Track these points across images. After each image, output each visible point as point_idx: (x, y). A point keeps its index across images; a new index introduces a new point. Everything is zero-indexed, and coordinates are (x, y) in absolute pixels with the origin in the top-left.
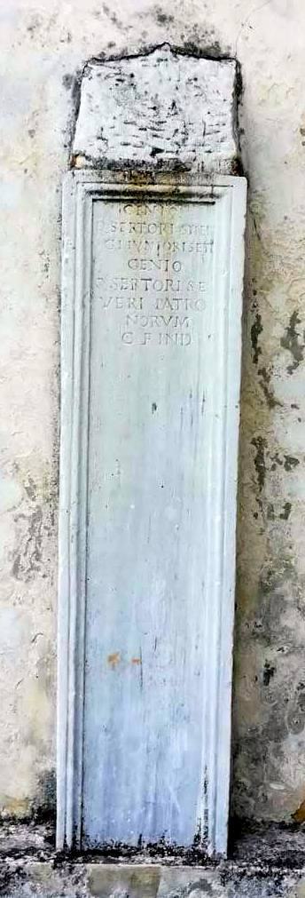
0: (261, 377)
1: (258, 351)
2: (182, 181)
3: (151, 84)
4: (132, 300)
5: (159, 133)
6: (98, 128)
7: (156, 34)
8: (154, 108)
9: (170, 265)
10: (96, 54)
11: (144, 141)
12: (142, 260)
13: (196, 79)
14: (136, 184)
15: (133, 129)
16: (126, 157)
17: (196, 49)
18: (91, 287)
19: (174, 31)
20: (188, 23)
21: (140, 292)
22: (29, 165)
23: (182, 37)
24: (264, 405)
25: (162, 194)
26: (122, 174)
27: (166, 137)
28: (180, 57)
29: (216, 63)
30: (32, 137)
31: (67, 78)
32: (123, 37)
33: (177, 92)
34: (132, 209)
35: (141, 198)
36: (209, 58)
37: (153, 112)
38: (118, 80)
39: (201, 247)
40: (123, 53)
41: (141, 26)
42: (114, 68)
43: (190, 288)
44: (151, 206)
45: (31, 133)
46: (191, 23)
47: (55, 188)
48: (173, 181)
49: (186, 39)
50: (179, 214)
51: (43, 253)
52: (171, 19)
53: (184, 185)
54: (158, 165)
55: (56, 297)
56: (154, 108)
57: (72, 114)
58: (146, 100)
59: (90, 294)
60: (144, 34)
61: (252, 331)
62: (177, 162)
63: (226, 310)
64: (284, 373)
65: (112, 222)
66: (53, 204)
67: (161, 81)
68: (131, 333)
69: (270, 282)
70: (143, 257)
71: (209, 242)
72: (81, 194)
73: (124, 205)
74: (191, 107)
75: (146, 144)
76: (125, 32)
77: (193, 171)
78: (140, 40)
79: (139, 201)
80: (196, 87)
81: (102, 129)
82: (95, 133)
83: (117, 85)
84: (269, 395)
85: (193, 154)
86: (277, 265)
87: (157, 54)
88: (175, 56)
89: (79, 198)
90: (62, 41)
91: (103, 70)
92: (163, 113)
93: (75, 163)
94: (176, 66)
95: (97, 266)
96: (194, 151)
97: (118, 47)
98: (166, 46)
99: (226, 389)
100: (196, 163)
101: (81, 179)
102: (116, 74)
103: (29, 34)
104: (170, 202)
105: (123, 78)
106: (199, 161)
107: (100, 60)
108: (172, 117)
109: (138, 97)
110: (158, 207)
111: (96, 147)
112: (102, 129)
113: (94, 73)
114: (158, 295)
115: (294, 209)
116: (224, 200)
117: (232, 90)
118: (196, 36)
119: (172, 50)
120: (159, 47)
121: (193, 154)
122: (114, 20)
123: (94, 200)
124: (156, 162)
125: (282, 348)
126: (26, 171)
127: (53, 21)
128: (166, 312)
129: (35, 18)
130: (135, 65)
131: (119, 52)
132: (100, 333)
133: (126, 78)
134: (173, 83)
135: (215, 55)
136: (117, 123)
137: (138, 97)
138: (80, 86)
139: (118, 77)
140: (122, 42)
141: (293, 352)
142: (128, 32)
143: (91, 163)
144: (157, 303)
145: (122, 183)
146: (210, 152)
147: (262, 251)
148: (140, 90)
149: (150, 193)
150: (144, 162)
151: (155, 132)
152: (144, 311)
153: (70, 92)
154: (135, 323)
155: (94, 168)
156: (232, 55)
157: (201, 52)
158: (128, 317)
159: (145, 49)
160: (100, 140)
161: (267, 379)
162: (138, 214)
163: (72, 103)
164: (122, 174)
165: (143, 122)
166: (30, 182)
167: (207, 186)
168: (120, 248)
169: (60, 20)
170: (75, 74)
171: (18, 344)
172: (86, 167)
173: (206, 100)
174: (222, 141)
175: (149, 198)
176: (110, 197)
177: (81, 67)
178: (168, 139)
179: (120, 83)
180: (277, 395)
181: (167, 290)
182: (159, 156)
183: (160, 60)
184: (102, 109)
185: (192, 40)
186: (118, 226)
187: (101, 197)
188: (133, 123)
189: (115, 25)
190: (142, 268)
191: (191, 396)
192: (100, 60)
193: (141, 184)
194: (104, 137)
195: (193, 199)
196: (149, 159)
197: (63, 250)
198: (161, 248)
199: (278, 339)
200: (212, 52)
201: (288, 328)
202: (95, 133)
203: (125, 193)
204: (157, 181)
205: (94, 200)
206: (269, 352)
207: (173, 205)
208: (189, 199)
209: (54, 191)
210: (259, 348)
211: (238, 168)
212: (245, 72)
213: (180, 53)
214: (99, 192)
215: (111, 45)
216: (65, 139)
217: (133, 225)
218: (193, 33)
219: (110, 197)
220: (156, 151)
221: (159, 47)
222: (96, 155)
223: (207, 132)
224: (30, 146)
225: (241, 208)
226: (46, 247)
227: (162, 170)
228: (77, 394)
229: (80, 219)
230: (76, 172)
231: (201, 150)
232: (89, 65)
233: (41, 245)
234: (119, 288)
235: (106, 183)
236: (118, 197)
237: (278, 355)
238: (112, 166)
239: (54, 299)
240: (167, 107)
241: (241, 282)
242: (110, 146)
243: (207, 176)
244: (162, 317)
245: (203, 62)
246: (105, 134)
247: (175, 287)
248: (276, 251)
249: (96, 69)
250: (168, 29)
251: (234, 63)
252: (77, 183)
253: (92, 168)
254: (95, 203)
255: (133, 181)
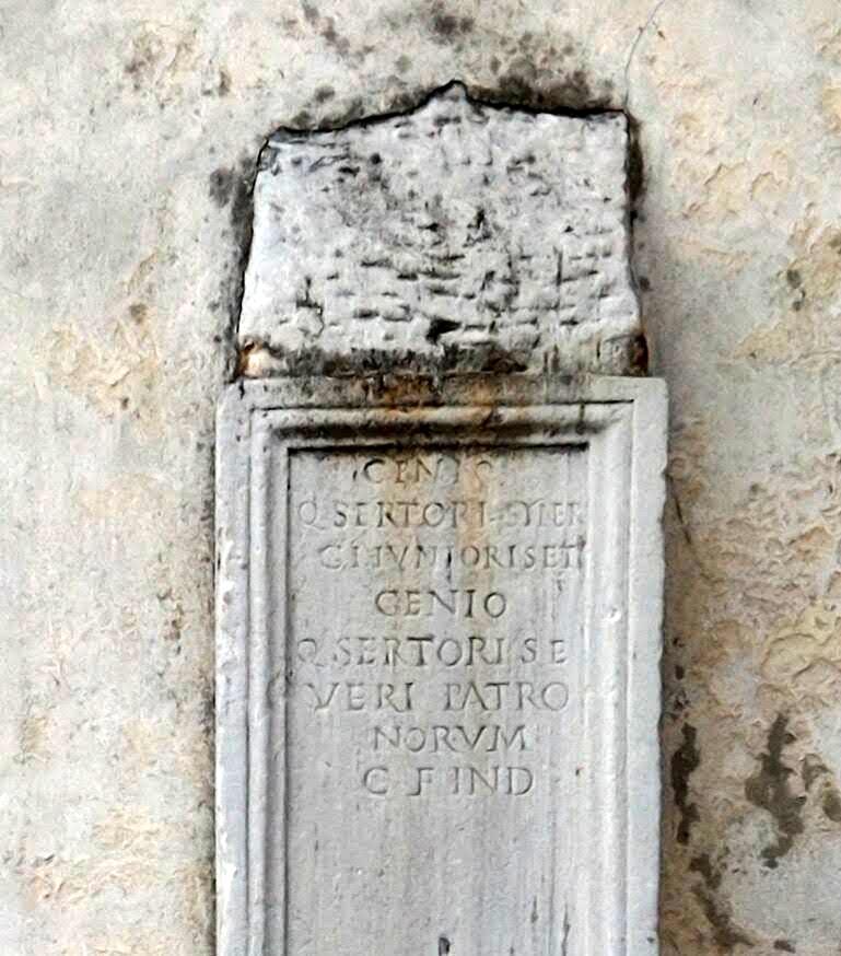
0: (698, 877)
1: (690, 814)
2: (508, 393)
3: (424, 174)
4: (386, 689)
5: (448, 284)
6: (299, 278)
7: (431, 62)
8: (433, 227)
9: (476, 598)
10: (283, 114)
11: (413, 305)
12: (409, 593)
13: (531, 160)
14: (393, 407)
15: (384, 279)
16: (368, 344)
17: (528, 92)
18: (288, 659)
19: (473, 54)
20: (509, 33)
21: (407, 671)
22: (133, 388)
23: (495, 65)
24: (706, 944)
25: (459, 428)
26: (358, 384)
27: (463, 290)
28: (490, 112)
29: (578, 122)
30: (139, 321)
31: (220, 180)
32: (352, 74)
33: (486, 190)
34: (383, 470)
35: (405, 440)
36: (561, 110)
37: (429, 236)
38: (345, 170)
39: (555, 555)
40: (352, 111)
41: (396, 45)
42: (332, 146)
43: (529, 655)
44: (430, 461)
45: (137, 312)
46: (517, 31)
47: (193, 438)
48: (483, 395)
49: (503, 70)
50: (493, 477)
51: (168, 595)
52: (467, 25)
53: (511, 404)
54: (445, 358)
55: (199, 698)
56: (433, 227)
57: (233, 263)
58: (414, 210)
59: (284, 679)
60: (403, 64)
61: (679, 764)
62: (493, 350)
63: (620, 706)
64: (757, 865)
65: (336, 502)
66: (191, 478)
67: (446, 166)
68: (385, 769)
69: (718, 645)
70: (410, 583)
71: (574, 541)
72: (260, 437)
73: (362, 461)
74: (523, 222)
75: (416, 311)
76: (355, 61)
77: (533, 370)
78: (393, 79)
79: (400, 449)
80: (532, 176)
81: (309, 282)
82: (290, 291)
83: (341, 180)
84: (717, 917)
85: (530, 329)
86: (735, 603)
87: (435, 108)
88: (480, 113)
89: (257, 454)
90: (208, 93)
91: (311, 151)
92: (457, 238)
93: (245, 366)
94: (484, 134)
95: (300, 612)
96: (534, 322)
97: (340, 97)
98: (456, 90)
99: (622, 899)
100: (539, 352)
101: (262, 400)
102: (336, 158)
103: (129, 82)
104: (477, 448)
105: (354, 165)
106: (546, 346)
107: (298, 131)
108: (479, 245)
109: (393, 204)
110: (448, 462)
111: (293, 323)
112: (309, 282)
113: (284, 160)
114: (451, 675)
115: (775, 468)
116: (613, 435)
117: (623, 178)
118: (528, 61)
119: (469, 99)
120: (439, 92)
121: (530, 329)
122: (330, 35)
123: (292, 452)
124: (440, 352)
125: (750, 806)
126: (125, 402)
127: (184, 47)
128: (468, 716)
129: (142, 41)
130: (382, 137)
131: (342, 110)
132: (313, 768)
133: (361, 165)
134: (476, 169)
135: (580, 104)
136: (348, 268)
137: (393, 204)
138: (251, 194)
139: (343, 163)
140: (346, 83)
141: (775, 815)
142: (363, 60)
143: (284, 365)
144: (448, 695)
145: (358, 407)
146: (573, 322)
147: (697, 571)
148: (398, 188)
149: (426, 428)
150: (411, 355)
151: (437, 282)
152: (417, 715)
153: (227, 211)
154: (394, 743)
155: (292, 374)
156: (616, 102)
157: (541, 98)
158: (377, 730)
159: (405, 100)
160: (304, 310)
161: (714, 881)
162: (398, 480)
163: (231, 238)
164: (358, 384)
165: (408, 259)
166: (136, 431)
167: (567, 403)
168: (355, 565)
169: (203, 44)
170: (239, 169)
171: (122, 256)
172: (272, 373)
173: (559, 203)
174: (603, 296)
175: (424, 440)
176: (331, 443)
177: (253, 151)
178: (471, 297)
179: (349, 179)
180: (738, 921)
181: (470, 662)
182: (450, 337)
183: (441, 121)
184: (308, 234)
185: (521, 72)
186: (348, 512)
187: (309, 443)
188: (385, 263)
189: (332, 49)
190: (408, 612)
191: (534, 918)
192: (298, 131)
193: (406, 406)
194: (313, 299)
195: (537, 439)
196: (424, 347)
197: (220, 576)
198: (456, 564)
199: (738, 784)
200: (568, 97)
201: (763, 756)
202: (290, 290)
203: (367, 429)
204: (444, 397)
205: (292, 452)
206: (717, 815)
207: (485, 457)
208: (524, 440)
209: (193, 446)
210: (693, 806)
211: (640, 356)
212: (653, 136)
213: (489, 105)
214: (306, 431)
215: (324, 95)
216: (215, 322)
217: (385, 509)
218: (519, 55)
219: (331, 443)
220: (440, 327)
221: (439, 92)
222: (294, 343)
223: (564, 275)
224: (134, 344)
225: (652, 459)
226: (174, 580)
227: (456, 371)
228: (257, 916)
229: (258, 493)
230: (247, 383)
231: (551, 321)
232: (272, 144)
233: (164, 575)
234: (354, 660)
235: (319, 407)
236: (349, 442)
237: (741, 820)
238: (334, 367)
239: (195, 702)
240: (463, 223)
241: (656, 635)
242: (327, 322)
243: (567, 380)
244: (460, 728)
245: (549, 121)
246: (321, 292)
247: (492, 655)
248: (732, 569)
249: (288, 151)
250: (459, 49)
251: (622, 120)
252: (252, 410)
253: (284, 374)
254: (296, 461)
255: (386, 398)
